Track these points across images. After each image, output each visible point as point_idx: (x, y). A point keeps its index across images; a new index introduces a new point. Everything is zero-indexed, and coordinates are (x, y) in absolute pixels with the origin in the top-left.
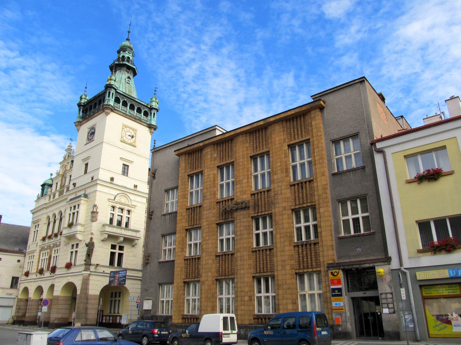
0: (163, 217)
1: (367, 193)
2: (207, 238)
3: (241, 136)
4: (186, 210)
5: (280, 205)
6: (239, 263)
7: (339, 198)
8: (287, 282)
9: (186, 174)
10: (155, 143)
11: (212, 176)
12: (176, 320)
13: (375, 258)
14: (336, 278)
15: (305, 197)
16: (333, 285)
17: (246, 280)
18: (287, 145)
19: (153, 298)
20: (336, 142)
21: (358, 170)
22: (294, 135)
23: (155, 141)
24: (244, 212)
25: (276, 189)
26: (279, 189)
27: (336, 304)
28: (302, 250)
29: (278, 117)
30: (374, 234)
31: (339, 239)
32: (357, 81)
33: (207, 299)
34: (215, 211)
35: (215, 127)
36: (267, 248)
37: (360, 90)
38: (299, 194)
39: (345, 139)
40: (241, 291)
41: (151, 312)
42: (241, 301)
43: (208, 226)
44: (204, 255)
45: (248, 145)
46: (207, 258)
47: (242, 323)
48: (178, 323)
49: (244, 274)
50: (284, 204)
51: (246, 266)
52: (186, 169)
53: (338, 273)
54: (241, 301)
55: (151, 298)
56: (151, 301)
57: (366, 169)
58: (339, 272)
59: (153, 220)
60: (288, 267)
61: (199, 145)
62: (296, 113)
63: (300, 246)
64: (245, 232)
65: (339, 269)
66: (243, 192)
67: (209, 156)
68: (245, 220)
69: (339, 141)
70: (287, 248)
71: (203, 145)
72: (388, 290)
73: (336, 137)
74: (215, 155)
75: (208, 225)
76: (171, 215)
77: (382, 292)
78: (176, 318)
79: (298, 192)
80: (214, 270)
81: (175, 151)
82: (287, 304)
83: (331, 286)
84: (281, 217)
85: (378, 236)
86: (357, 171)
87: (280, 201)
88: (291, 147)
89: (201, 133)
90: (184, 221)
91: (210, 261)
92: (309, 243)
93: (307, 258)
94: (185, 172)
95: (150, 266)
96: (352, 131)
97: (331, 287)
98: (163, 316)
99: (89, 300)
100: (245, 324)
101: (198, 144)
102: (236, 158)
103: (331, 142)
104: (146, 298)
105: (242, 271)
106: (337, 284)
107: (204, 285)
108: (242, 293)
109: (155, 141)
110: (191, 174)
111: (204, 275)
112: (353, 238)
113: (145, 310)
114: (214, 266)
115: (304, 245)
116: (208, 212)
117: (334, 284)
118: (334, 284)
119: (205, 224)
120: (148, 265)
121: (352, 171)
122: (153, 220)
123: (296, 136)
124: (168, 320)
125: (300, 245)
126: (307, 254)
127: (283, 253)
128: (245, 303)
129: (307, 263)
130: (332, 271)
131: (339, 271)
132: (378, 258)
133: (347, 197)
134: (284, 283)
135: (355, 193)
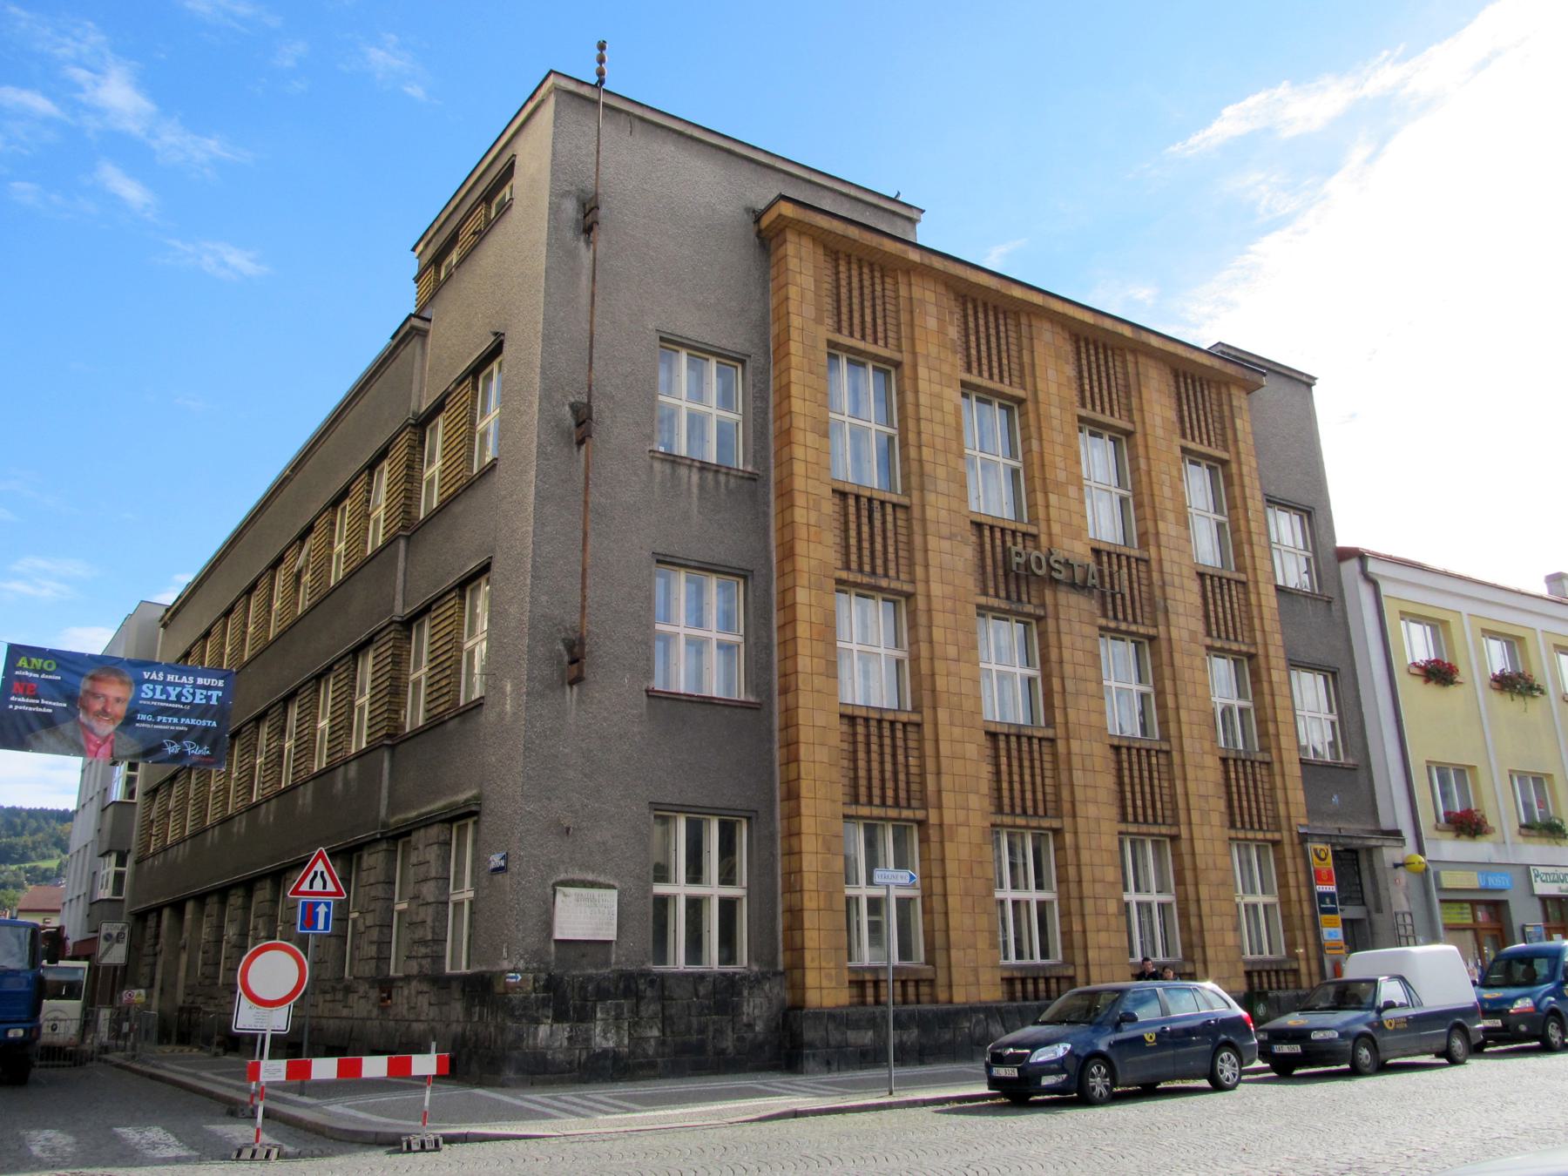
0: (657, 465)
10: (601, 60)
11: (948, 407)
12: (825, 992)
19: (617, 876)
23: (602, 46)
29: (1170, 347)
35: (915, 211)
40: (1094, 881)
41: (608, 953)
43: (949, 604)
48: (838, 1007)
49: (1098, 820)
56: (615, 893)
65: (1327, 843)
72: (1406, 908)
78: (825, 983)
82: (1222, 929)
84: (1187, 661)
89: (853, 192)
95: (580, 701)
98: (701, 977)
101: (899, 246)
104: (562, 876)
108: (1099, 888)
109: (602, 46)
113: (557, 941)
116: (946, 545)
119: (936, 589)
120: (572, 694)
124: (740, 994)
134: (1211, 864)
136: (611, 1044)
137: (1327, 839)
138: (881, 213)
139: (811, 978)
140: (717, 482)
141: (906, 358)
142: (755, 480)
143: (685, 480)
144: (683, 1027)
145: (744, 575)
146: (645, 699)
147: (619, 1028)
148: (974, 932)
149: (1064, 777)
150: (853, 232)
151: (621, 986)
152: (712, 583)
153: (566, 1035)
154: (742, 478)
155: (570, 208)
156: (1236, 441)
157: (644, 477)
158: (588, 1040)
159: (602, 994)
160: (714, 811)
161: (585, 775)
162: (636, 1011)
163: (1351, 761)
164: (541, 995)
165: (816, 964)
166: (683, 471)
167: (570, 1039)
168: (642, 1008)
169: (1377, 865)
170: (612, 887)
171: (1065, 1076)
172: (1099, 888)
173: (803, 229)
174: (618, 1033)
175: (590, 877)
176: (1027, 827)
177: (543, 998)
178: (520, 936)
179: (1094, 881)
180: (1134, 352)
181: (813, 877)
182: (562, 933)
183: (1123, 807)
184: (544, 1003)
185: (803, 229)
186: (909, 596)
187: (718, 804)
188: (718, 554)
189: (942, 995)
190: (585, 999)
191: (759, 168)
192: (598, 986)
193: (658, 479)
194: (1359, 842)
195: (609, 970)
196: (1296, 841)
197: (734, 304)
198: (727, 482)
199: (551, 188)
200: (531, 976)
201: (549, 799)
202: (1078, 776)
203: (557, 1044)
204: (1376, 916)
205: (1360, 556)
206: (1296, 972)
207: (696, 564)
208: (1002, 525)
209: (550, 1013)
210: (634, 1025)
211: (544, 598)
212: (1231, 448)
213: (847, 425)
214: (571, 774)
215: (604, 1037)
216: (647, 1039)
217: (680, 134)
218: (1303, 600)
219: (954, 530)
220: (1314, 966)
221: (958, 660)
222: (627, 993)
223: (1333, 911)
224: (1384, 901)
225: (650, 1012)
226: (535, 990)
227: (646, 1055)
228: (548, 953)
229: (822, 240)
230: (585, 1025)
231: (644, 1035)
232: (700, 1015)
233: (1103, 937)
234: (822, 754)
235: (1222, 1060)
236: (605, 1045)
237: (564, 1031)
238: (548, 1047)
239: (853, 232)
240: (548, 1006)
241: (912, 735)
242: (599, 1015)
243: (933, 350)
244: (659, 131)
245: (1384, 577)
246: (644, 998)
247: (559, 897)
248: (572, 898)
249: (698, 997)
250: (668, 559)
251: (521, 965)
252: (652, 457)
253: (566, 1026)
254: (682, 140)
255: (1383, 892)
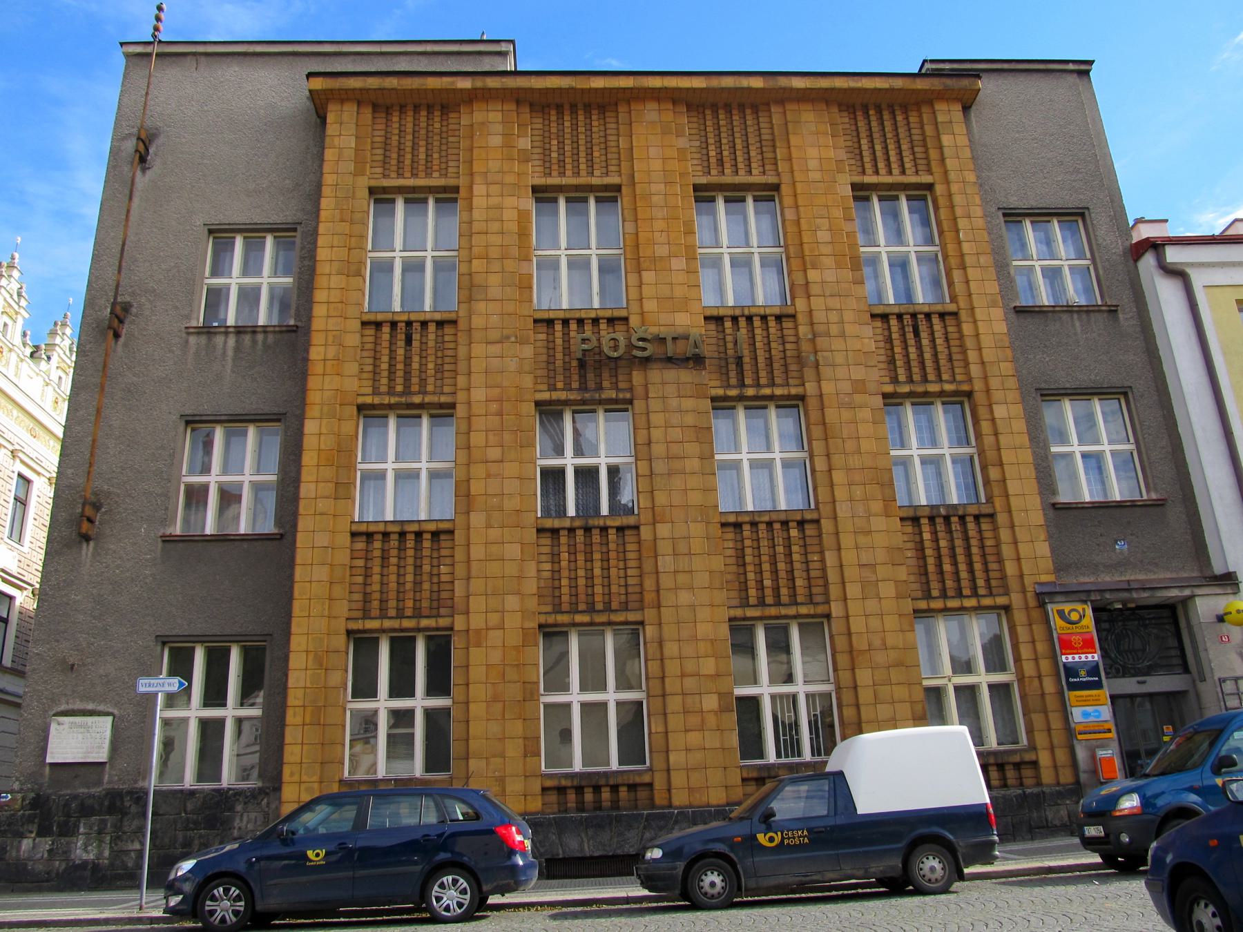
0: (193, 340)
1: (1129, 384)
2: (494, 453)
3: (652, 105)
4: (359, 325)
5: (841, 372)
6: (666, 563)
7: (1043, 386)
8: (889, 642)
9: (364, 182)
11: (510, 215)
13: (1174, 575)
14: (1078, 631)
15: (929, 364)
16: (1068, 651)
17: (704, 629)
18: (849, 181)
20: (1013, 216)
21: (1097, 314)
22: (875, 160)
23: (160, 8)
24: (686, 376)
25: (819, 316)
26: (833, 317)
27: (1086, 714)
28: (934, 533)
29: (824, 83)
30: (1162, 505)
31: (1056, 509)
32: (1071, 67)
33: (499, 706)
34: (528, 351)
35: (503, 44)
36: (789, 518)
37: (1079, 94)
38: (906, 347)
39: (1041, 215)
40: (683, 675)
41: (103, 772)
42: (686, 712)
43: (494, 407)
44: (477, 519)
45: (682, 142)
46: (494, 533)
47: (696, 803)
49: (693, 607)
50: (858, 373)
51: (702, 579)
52: (359, 161)
53: (1082, 617)
54: (686, 712)
55: (101, 708)
56: (110, 719)
57: (1121, 316)
58: (1084, 609)
59: (125, 345)
60: (888, 590)
61: (453, 83)
62: (891, 90)
63: (924, 521)
64: (693, 448)
65: (1085, 602)
66: (684, 305)
67: (496, 141)
68: (688, 403)
69: (1019, 219)
70: (879, 523)
71: (474, 89)
73: (1014, 202)
74: (525, 143)
75: (500, 400)
76: (247, 338)
77: (1223, 676)
79: (905, 341)
80: (531, 587)
81: (310, 75)
83: (1064, 657)
84: (846, 415)
85: (1175, 514)
86: (1092, 315)
87: (839, 359)
88: (861, 192)
89: (429, 48)
90: (352, 368)
91: (513, 551)
92: (960, 513)
93: (955, 563)
94: (358, 173)
95: (96, 554)
96: (1069, 200)
97: (1096, 655)
99: (361, 599)
100: (708, 806)
101: (446, 80)
102: (633, 176)
103: (1000, 214)
104: (63, 707)
105: (685, 597)
106: (1081, 648)
107: (478, 645)
108: (690, 683)
110: (385, 190)
111: (476, 604)
112: (1101, 512)
113: (52, 765)
114: (531, 569)
115: (939, 516)
116: (494, 349)
117: (1074, 648)
118: (1074, 648)
119: (478, 394)
120: (88, 550)
121: (1078, 312)
122: (125, 345)
123: (881, 165)
124: (231, 809)
125: (924, 517)
126: (952, 549)
127: (862, 540)
128: (703, 721)
129: (958, 580)
130: (1060, 607)
131: (1085, 606)
132: (1180, 575)
133: (1068, 386)
134: (877, 642)
135: (1093, 377)
136: (92, 857)
137: (1083, 597)
138: (365, 57)
139: (1043, 776)
140: (254, 342)
141: (462, 182)
142: (295, 331)
143: (221, 345)
144: (167, 840)
145: (1121, 393)
146: (160, 545)
147: (101, 841)
148: (502, 739)
149: (648, 566)
150: (392, 82)
151: (106, 803)
152: (1097, 406)
153: (47, 847)
154: (281, 332)
155: (130, 145)
156: (942, 160)
157: (178, 352)
158: (67, 852)
159: (86, 810)
160: (200, 639)
161: (94, 618)
162: (118, 827)
163: (1154, 496)
164: (27, 813)
165: (296, 778)
166: (219, 339)
167: (50, 851)
168: (126, 823)
169: (1194, 622)
170: (107, 714)
171: (181, 896)
172: (690, 683)
173: (343, 96)
174: (99, 846)
175: (90, 706)
176: (419, 630)
177: (29, 815)
178: (18, 761)
179: (683, 675)
180: (781, 102)
181: (300, 693)
182: (53, 758)
183: (744, 588)
184: (30, 820)
185: (343, 96)
186: (969, 395)
187: (228, 631)
188: (250, 405)
189: (660, 799)
190: (68, 816)
191: (327, 58)
192: (82, 804)
193: (192, 350)
194: (1145, 595)
195: (99, 789)
196: (1032, 602)
197: (287, 182)
198: (265, 339)
199: (113, 135)
200: (19, 796)
201: (58, 641)
202: (665, 563)
203: (39, 856)
204: (1202, 687)
205: (1155, 246)
206: (1035, 764)
207: (226, 418)
208: (577, 315)
209: (35, 828)
210: (116, 839)
211: (70, 471)
212: (935, 167)
213: (911, 243)
214: (81, 617)
215: (83, 850)
216: (127, 852)
217: (245, 54)
218: (1065, 317)
219: (506, 332)
220: (1062, 756)
221: (502, 461)
222: (111, 810)
223: (1098, 685)
224: (1206, 670)
225: (133, 827)
226: (22, 808)
227: (125, 867)
228: (42, 775)
229: (360, 98)
230: (67, 839)
231: (125, 848)
232: (186, 829)
233: (694, 738)
234: (321, 573)
235: (442, 886)
236: (85, 856)
237: (46, 844)
238: (29, 859)
239: (392, 82)
240: (33, 822)
241: (985, 526)
242: (82, 830)
243: (494, 165)
244: (224, 59)
245: (1192, 265)
246: (126, 814)
247: (53, 727)
248: (66, 726)
249: (186, 812)
250: (197, 418)
251: (16, 786)
252: (188, 334)
253: (49, 840)
254: (248, 59)
255: (1202, 655)
